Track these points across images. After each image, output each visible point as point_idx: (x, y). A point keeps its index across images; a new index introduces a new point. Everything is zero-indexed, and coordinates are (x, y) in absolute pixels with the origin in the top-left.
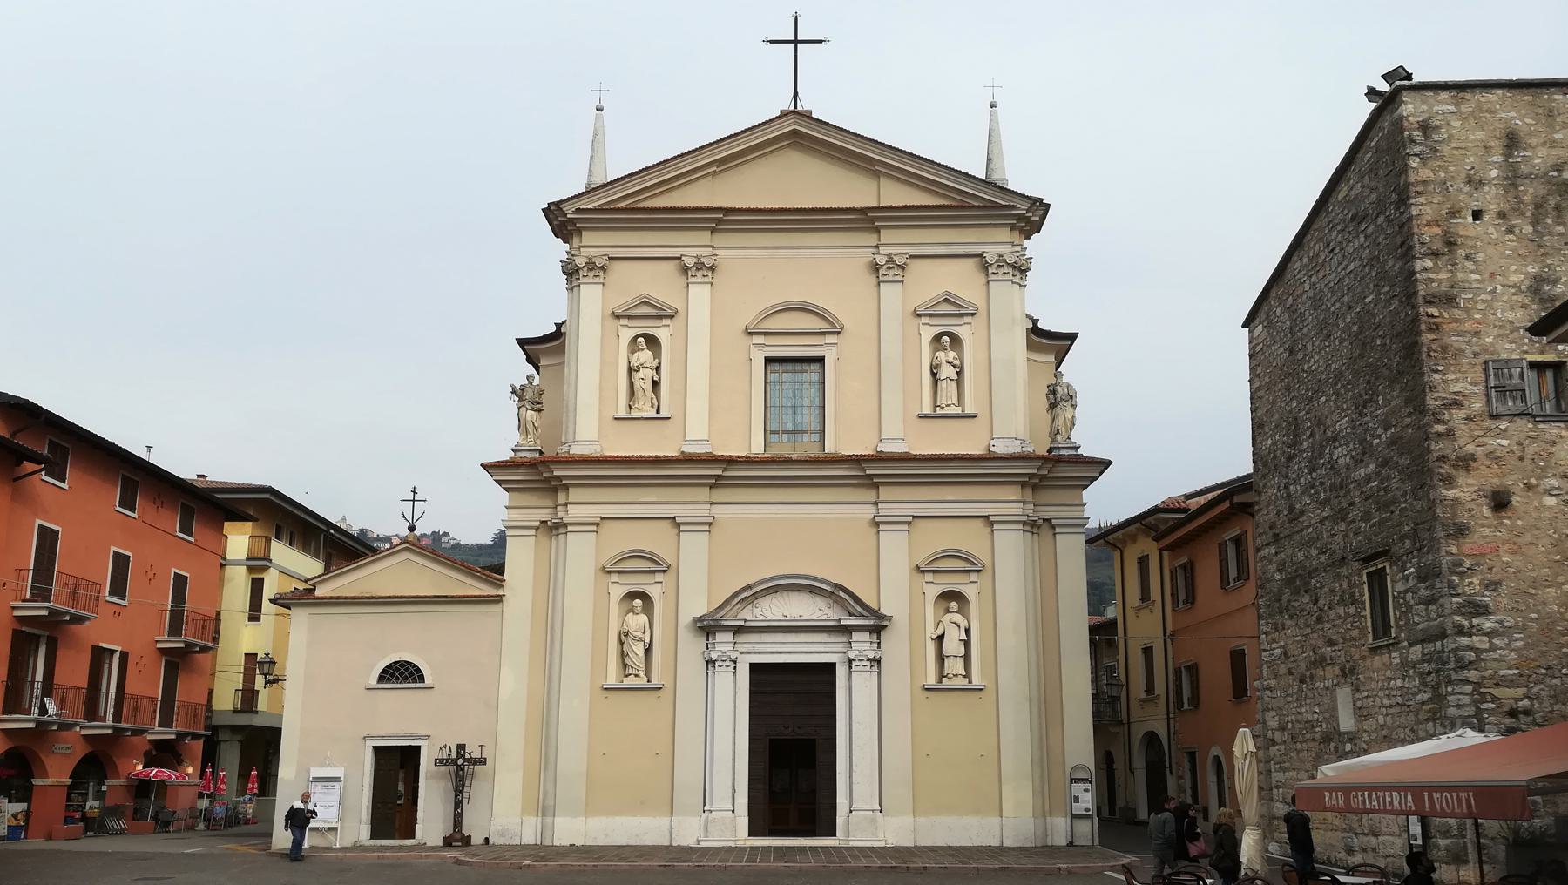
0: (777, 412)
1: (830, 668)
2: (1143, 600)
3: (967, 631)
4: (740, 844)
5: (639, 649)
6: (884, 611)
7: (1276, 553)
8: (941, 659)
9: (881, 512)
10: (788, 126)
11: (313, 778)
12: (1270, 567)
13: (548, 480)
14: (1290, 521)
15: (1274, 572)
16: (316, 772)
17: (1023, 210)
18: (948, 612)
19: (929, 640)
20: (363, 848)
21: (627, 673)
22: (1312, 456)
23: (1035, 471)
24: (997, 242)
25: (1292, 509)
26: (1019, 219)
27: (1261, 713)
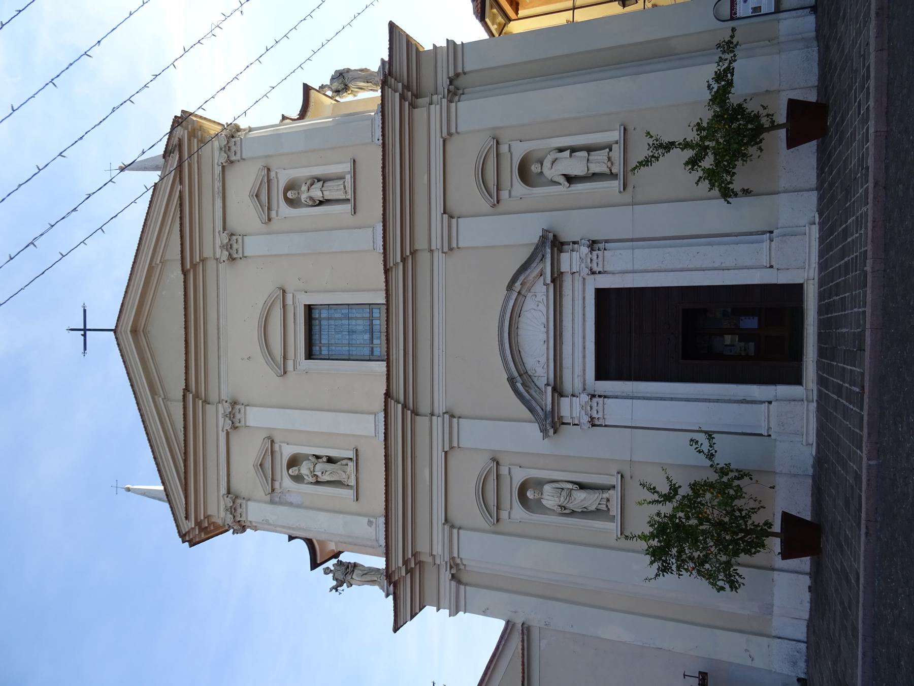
1: (602, 295)
3: (561, 150)
5: (581, 499)
6: (535, 239)
9: (439, 246)
10: (128, 339)
13: (410, 571)
17: (184, 133)
18: (541, 173)
19: (570, 189)
21: (606, 509)
23: (397, 95)
24: (213, 156)
26: (404, 99)
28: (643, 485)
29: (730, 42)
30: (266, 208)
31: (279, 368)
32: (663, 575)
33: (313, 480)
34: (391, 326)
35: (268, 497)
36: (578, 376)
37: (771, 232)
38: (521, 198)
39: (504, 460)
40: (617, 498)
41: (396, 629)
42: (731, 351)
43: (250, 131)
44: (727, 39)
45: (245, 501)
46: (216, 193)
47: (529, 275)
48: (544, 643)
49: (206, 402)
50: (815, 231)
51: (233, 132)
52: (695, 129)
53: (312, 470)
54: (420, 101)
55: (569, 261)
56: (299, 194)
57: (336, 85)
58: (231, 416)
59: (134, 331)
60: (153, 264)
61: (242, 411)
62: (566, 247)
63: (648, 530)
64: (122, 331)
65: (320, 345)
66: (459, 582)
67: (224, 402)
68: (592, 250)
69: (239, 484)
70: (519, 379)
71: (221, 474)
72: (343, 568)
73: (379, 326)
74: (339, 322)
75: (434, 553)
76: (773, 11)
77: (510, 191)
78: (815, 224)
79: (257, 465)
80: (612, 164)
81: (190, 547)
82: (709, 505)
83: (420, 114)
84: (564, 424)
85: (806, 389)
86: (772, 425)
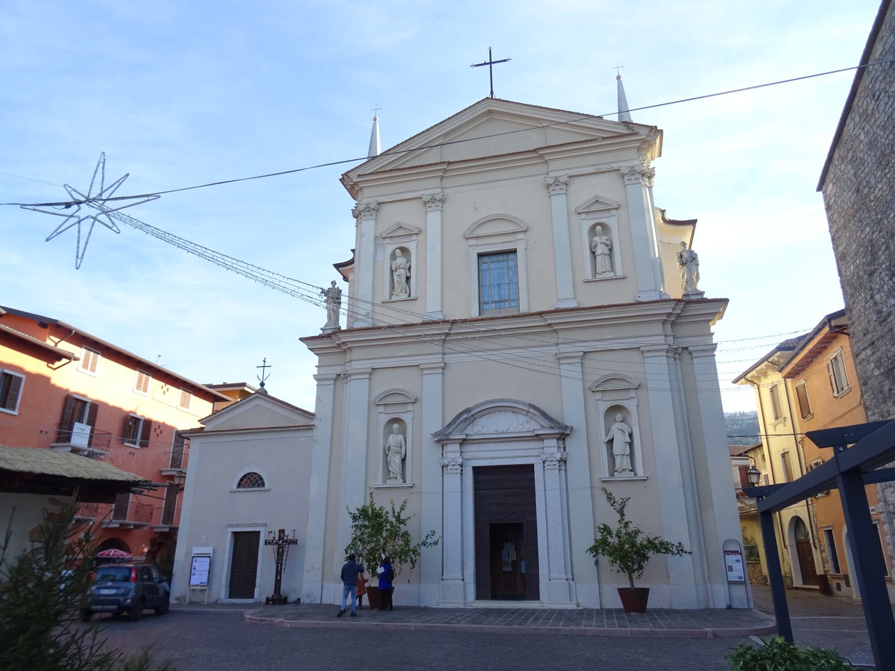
0: (487, 289)
1: (530, 468)
2: (777, 418)
3: (631, 435)
4: (468, 607)
5: (396, 460)
7: (873, 354)
8: (612, 457)
11: (194, 554)
12: (868, 366)
13: (339, 346)
14: (881, 323)
15: (873, 370)
16: (196, 550)
17: (644, 135)
20: (224, 605)
22: (890, 265)
23: (670, 311)
25: (879, 312)
27: (881, 493)
28: (405, 502)
29: (682, 551)
30: (588, 210)
31: (469, 234)
32: (351, 517)
33: (393, 268)
34: (501, 320)
35: (378, 235)
36: (475, 455)
37: (573, 580)
38: (596, 408)
39: (417, 406)
40: (397, 484)
41: (301, 339)
42: (505, 555)
43: (649, 187)
44: (685, 549)
45: (374, 218)
46: (598, 167)
47: (540, 418)
48: (303, 439)
49: (442, 178)
50: (573, 607)
51: (649, 175)
52: (636, 529)
53: (400, 267)
54: (669, 327)
55: (551, 447)
56: (599, 235)
57: (685, 255)
58: (433, 200)
59: (490, 112)
60: (542, 121)
61: (438, 208)
62: (561, 442)
63: (377, 506)
64: (489, 104)
65: (489, 262)
66: (335, 380)
67: (442, 193)
68: (559, 461)
69: (386, 210)
70: (470, 415)
71: (392, 196)
72: (336, 296)
73: (504, 307)
74: (506, 276)
75: (352, 362)
76: (729, 580)
77: (601, 400)
78: (578, 607)
79: (400, 224)
80: (620, 472)
81: (340, 180)
82: (394, 544)
83: (658, 328)
84: (443, 446)
85: (472, 602)
86: (448, 581)
